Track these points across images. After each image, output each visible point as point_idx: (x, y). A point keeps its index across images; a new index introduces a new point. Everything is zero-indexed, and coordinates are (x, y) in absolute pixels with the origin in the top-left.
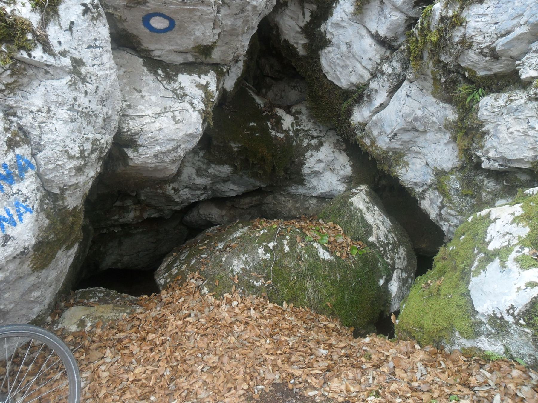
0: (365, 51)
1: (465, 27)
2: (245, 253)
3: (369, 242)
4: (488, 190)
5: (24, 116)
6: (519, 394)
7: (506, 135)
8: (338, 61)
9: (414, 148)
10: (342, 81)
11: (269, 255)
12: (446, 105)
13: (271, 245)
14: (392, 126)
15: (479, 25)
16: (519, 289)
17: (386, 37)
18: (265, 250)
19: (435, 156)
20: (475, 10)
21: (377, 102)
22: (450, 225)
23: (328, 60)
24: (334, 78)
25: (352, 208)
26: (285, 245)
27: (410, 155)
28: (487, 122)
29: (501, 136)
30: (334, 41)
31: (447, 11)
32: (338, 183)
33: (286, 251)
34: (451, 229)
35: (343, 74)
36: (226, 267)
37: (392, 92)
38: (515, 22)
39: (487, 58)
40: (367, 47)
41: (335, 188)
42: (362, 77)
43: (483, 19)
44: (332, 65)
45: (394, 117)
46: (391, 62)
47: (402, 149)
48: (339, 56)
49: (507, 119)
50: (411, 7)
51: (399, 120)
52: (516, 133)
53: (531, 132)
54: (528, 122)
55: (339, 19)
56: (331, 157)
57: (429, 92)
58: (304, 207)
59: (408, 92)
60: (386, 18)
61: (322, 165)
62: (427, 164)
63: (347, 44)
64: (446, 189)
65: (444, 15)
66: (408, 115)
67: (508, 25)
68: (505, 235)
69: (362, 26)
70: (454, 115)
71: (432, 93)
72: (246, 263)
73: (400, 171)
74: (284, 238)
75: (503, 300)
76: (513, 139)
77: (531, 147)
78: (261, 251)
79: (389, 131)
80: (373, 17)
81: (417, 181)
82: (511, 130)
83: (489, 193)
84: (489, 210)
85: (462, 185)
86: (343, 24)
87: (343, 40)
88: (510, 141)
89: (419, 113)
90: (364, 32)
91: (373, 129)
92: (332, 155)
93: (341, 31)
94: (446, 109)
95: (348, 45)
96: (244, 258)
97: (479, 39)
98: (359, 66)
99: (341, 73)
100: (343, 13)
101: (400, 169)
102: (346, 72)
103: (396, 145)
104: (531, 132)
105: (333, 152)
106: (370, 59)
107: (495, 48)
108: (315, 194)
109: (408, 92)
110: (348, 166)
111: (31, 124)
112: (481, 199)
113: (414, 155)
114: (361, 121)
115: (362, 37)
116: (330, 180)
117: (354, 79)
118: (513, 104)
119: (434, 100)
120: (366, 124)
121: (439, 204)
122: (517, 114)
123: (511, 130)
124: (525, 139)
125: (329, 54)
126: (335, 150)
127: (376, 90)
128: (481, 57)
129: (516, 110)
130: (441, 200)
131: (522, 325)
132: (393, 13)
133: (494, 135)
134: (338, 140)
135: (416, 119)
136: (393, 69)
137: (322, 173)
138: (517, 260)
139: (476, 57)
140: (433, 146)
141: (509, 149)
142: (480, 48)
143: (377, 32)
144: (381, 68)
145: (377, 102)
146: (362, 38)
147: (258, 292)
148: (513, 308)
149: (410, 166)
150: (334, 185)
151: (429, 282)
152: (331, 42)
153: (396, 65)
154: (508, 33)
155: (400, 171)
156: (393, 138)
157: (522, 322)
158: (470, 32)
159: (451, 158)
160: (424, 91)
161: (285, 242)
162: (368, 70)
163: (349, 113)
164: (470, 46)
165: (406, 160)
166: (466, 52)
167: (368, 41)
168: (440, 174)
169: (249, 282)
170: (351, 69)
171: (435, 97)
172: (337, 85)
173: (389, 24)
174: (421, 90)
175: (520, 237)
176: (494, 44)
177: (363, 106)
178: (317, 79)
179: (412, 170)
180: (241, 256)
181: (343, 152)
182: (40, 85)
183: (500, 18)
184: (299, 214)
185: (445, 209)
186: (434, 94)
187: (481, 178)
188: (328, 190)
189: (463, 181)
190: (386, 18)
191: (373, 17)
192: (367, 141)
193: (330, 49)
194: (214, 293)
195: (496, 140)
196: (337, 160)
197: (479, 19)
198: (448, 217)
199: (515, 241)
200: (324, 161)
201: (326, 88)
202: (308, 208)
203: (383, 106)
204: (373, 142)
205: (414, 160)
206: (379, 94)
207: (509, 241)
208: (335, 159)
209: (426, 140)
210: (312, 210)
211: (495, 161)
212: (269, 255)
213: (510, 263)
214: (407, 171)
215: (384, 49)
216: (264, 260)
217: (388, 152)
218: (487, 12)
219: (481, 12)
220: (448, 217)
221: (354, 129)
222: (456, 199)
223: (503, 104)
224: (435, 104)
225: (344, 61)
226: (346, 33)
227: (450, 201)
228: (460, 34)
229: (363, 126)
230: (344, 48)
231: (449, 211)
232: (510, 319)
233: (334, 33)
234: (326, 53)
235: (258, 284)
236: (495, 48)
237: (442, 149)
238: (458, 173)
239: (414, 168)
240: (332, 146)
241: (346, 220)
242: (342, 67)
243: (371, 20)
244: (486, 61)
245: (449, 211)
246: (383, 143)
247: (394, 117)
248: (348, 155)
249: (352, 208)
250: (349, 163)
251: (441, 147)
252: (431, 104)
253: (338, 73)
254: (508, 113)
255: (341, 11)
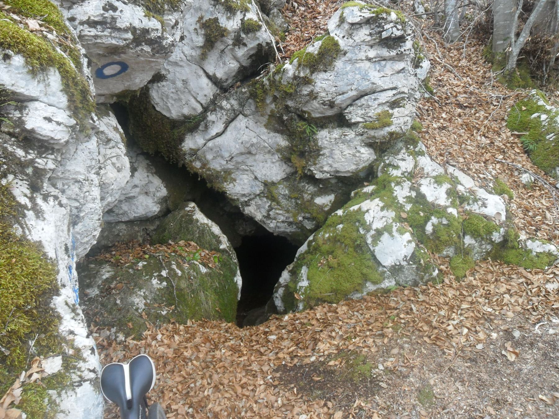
0: (202, 89)
1: (314, 86)
2: (140, 289)
3: (221, 249)
4: (309, 192)
5: (66, 187)
6: (419, 300)
7: (340, 157)
8: (172, 95)
9: (243, 166)
10: (172, 112)
11: (165, 283)
12: (277, 134)
13: (164, 273)
14: (231, 151)
15: (324, 86)
16: (405, 246)
17: (221, 79)
18: (159, 280)
19: (264, 172)
20: (321, 75)
21: (214, 131)
22: (278, 222)
23: (160, 93)
24: (163, 109)
25: (199, 224)
26: (177, 270)
27: (237, 173)
28: (325, 148)
29: (336, 157)
30: (169, 76)
31: (299, 73)
32: (154, 204)
33: (180, 275)
34: (279, 224)
35: (175, 106)
36: (127, 307)
37: (227, 124)
38: (349, 87)
39: (326, 107)
40: (204, 85)
41: (151, 210)
42: (194, 109)
43: (327, 82)
44: (164, 98)
45: (232, 144)
46: (229, 100)
47: (232, 169)
48: (174, 91)
49: (341, 147)
50: (246, 58)
51: (238, 147)
52: (348, 155)
53: (358, 154)
54: (356, 148)
55: (178, 59)
56: (145, 181)
57: (263, 124)
58: (112, 235)
59: (247, 124)
60: (224, 63)
61: (138, 190)
62: (256, 178)
63: (183, 81)
64: (276, 196)
65: (296, 74)
66: (247, 142)
67: (345, 89)
68: (382, 218)
69: (199, 67)
70: (284, 142)
71: (265, 125)
72: (145, 298)
73: (228, 187)
74: (171, 264)
75: (399, 254)
76: (346, 158)
77: (355, 163)
78: (155, 281)
79: (227, 155)
80: (212, 62)
81: (246, 192)
82: (345, 153)
83: (309, 194)
84: (359, 205)
85: (290, 191)
86: (181, 63)
87: (179, 77)
88: (343, 160)
89: (255, 141)
90: (201, 73)
91: (207, 154)
92: (146, 179)
93: (178, 69)
94: (276, 137)
95: (185, 82)
96: (142, 293)
97: (323, 94)
98: (193, 100)
99: (172, 105)
100: (182, 54)
101: (228, 185)
102: (178, 104)
103: (230, 166)
104: (358, 154)
105: (148, 176)
106: (205, 96)
107: (334, 101)
108: (125, 219)
109: (247, 124)
110: (163, 188)
111: (77, 195)
112: (303, 199)
113: (241, 173)
114: (193, 147)
115: (199, 76)
116: (145, 203)
117: (186, 111)
118: (347, 137)
119: (266, 130)
120: (198, 150)
121: (267, 207)
122: (350, 143)
123: (345, 153)
124: (352, 159)
125: (163, 88)
126: (149, 174)
127: (214, 122)
128: (322, 106)
129: (350, 141)
130: (269, 204)
131: (411, 265)
132: (232, 61)
133: (329, 156)
134: (147, 164)
135: (252, 145)
136: (232, 106)
137: (137, 197)
138: (397, 231)
139: (318, 105)
140: (261, 164)
141: (342, 165)
142: (323, 100)
143: (214, 75)
144: (221, 104)
145: (214, 131)
146: (200, 78)
147: (166, 319)
148: (406, 256)
149: (237, 181)
150: (150, 207)
151: (322, 261)
152: (165, 77)
153: (233, 102)
154: (343, 94)
155: (228, 187)
156: (230, 161)
157: (411, 263)
158: (317, 89)
159: (279, 172)
160: (258, 123)
161: (174, 267)
162: (201, 105)
163: (181, 140)
164: (316, 98)
165: (233, 177)
166: (312, 102)
167: (205, 81)
168: (268, 185)
169: (158, 314)
170: (184, 103)
171: (266, 128)
172: (165, 116)
173: (227, 69)
174: (256, 123)
175: (392, 218)
176: (334, 100)
177: (196, 134)
178: (146, 109)
179: (239, 184)
180: (139, 293)
181: (155, 175)
182: (77, 149)
183: (339, 84)
184: (111, 242)
185: (273, 210)
186: (266, 126)
187: (303, 184)
188: (144, 213)
189: (291, 188)
190: (224, 63)
191: (212, 62)
192: (198, 165)
193: (164, 83)
194: (133, 336)
195: (331, 159)
196: (152, 183)
197: (323, 82)
198: (276, 216)
199: (391, 221)
200: (139, 185)
201: (154, 118)
202: (118, 235)
203: (218, 135)
204: (204, 165)
205: (241, 176)
206: (215, 125)
207: (387, 221)
208: (150, 182)
209: (255, 161)
210: (123, 235)
211: (328, 173)
212: (165, 283)
213: (395, 233)
214: (234, 185)
215: (216, 88)
216: (160, 290)
217: (221, 172)
218: (330, 78)
219: (326, 78)
220: (276, 216)
221: (185, 154)
222: (284, 202)
223: (337, 137)
224: (267, 134)
225: (178, 95)
226: (183, 71)
227: (278, 203)
228: (309, 90)
229: (194, 152)
230: (179, 84)
231: (277, 211)
232: (404, 263)
233: (170, 70)
234: (159, 87)
235: (164, 313)
236: (334, 101)
237: (270, 166)
238: (285, 183)
239: (242, 183)
240: (145, 171)
241: (197, 235)
242: (175, 100)
243: (210, 63)
244: (324, 109)
245: (277, 211)
246: (216, 165)
247: (232, 144)
248: (160, 177)
249: (199, 224)
250: (162, 185)
251: (268, 165)
252: (264, 134)
253: (169, 105)
254: (342, 143)
255: (180, 52)
